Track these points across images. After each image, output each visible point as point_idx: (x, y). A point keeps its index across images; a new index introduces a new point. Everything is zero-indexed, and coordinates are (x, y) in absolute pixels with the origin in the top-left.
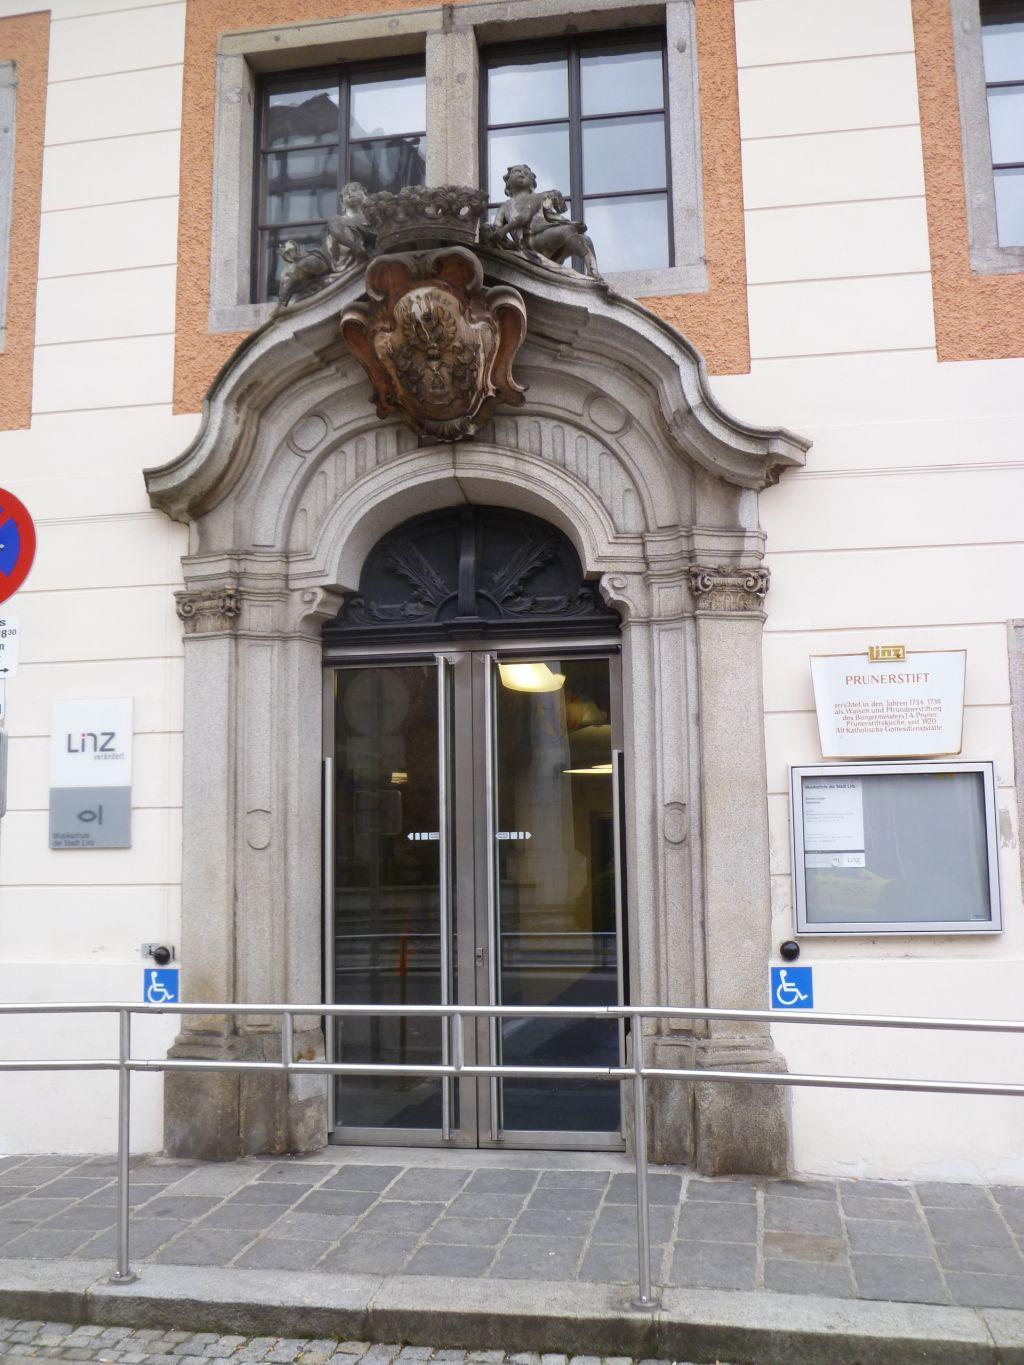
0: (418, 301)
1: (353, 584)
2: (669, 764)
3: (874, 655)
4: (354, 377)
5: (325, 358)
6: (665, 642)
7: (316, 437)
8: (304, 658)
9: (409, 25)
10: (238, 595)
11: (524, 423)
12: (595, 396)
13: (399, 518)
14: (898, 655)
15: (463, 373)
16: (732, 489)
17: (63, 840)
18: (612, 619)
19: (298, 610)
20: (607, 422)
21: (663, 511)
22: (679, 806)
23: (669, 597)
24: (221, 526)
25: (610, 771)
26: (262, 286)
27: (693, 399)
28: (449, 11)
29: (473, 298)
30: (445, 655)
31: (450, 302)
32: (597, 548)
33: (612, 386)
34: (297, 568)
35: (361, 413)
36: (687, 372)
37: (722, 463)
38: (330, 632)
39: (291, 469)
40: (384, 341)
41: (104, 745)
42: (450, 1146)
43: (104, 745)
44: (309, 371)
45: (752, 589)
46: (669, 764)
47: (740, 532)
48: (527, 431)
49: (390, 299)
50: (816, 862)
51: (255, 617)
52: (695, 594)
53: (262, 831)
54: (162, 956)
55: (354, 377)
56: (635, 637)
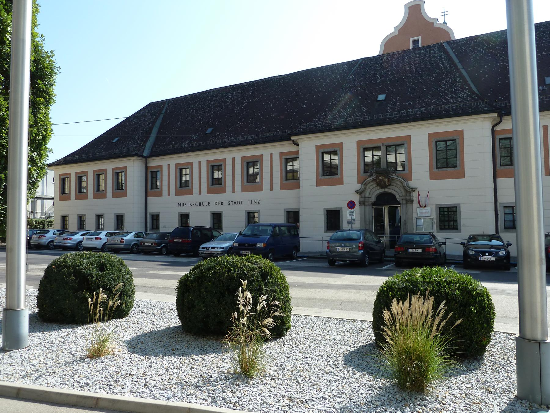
0: (381, 178)
1: (375, 162)
4: (375, 182)
5: (372, 181)
6: (404, 206)
10: (365, 202)
11: (391, 186)
13: (385, 41)
19: (370, 203)
21: (404, 194)
22: (405, 221)
23: (404, 202)
24: (363, 195)
26: (365, 172)
28: (383, 144)
30: (384, 206)
31: (384, 178)
32: (398, 198)
34: (370, 199)
35: (375, 185)
38: (373, 204)
40: (378, 181)
44: (371, 182)
47: (411, 196)
48: (391, 187)
49: (378, 177)
51: (366, 203)
52: (406, 202)
53: (367, 223)
55: (375, 182)
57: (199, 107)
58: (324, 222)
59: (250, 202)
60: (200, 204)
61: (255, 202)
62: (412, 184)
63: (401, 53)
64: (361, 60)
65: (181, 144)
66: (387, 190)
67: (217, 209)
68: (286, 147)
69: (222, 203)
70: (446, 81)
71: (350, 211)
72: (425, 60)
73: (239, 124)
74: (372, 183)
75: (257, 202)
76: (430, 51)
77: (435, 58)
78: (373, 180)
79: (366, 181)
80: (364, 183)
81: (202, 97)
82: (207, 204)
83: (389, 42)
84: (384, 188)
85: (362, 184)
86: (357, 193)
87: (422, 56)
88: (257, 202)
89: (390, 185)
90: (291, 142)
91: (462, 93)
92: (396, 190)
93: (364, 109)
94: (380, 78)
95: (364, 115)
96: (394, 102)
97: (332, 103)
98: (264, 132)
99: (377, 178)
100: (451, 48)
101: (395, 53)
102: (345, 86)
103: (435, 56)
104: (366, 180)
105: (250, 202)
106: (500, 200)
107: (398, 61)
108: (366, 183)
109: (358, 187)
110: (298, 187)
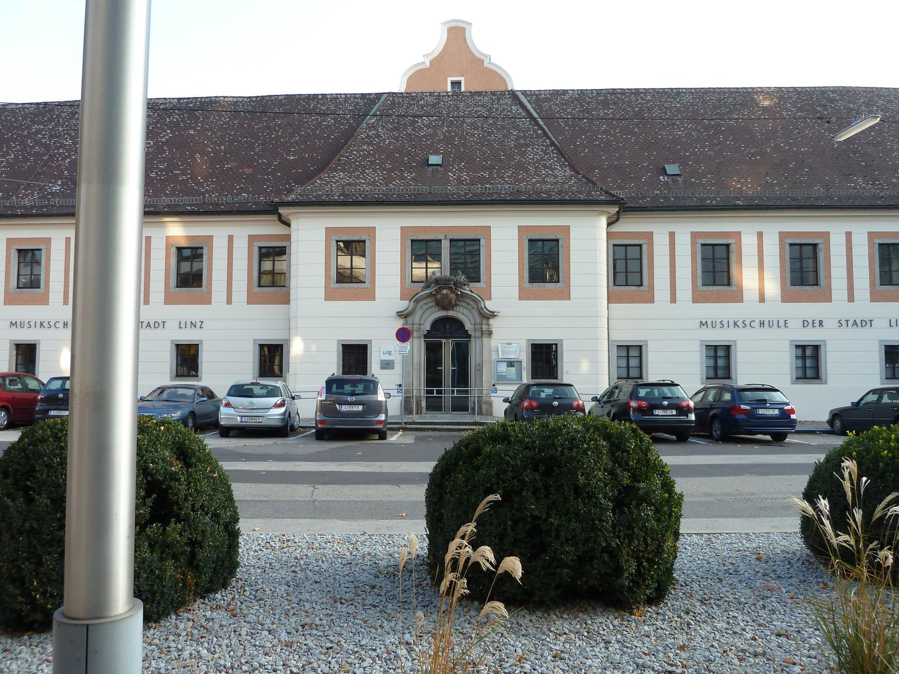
0: (445, 291)
2: (478, 358)
3: (507, 344)
5: (428, 296)
6: (478, 341)
7: (425, 307)
8: (423, 340)
9: (439, 238)
12: (468, 304)
13: (500, 72)
14: (511, 344)
15: (450, 301)
16: (488, 318)
17: (382, 368)
18: (470, 336)
20: (470, 307)
22: (479, 365)
23: (478, 334)
24: (410, 320)
25: (687, 239)
27: (483, 307)
28: (445, 236)
29: (452, 292)
30: (443, 341)
32: (468, 326)
33: (471, 303)
34: (422, 327)
35: (434, 304)
36: (482, 302)
37: (487, 315)
38: (425, 336)
39: (421, 311)
40: (439, 296)
41: (390, 353)
42: (443, 414)
43: (390, 353)
44: (426, 298)
45: (490, 333)
46: (478, 358)
47: (489, 325)
48: (458, 308)
50: (498, 374)
52: (482, 334)
54: (400, 386)
56: (473, 340)
57: (58, 130)
58: (338, 366)
59: (183, 325)
60: (762, 324)
61: (193, 325)
62: (490, 305)
63: (452, 96)
64: (386, 95)
65: (22, 198)
66: (451, 313)
67: (809, 336)
68: (266, 228)
69: (821, 323)
70: (533, 149)
71: (400, 345)
72: (493, 112)
73: (156, 173)
74: (427, 301)
75: (198, 324)
76: (499, 99)
77: (508, 112)
78: (430, 295)
79: (418, 296)
80: (413, 300)
81: (64, 112)
82: (782, 324)
83: (417, 76)
84: (447, 310)
85: (410, 301)
86: (400, 316)
87: (487, 106)
88: (198, 324)
89: (457, 305)
90: (275, 217)
91: (560, 171)
92: (465, 316)
93: (409, 176)
94: (425, 129)
95: (411, 185)
96: (457, 170)
97: (347, 157)
98: (214, 193)
99: (438, 291)
100: (529, 102)
101: (442, 94)
102: (365, 132)
103: (507, 109)
104: (417, 294)
105: (183, 325)
106: (610, 339)
107: (450, 107)
108: (416, 300)
109: (403, 305)
110: (286, 300)
